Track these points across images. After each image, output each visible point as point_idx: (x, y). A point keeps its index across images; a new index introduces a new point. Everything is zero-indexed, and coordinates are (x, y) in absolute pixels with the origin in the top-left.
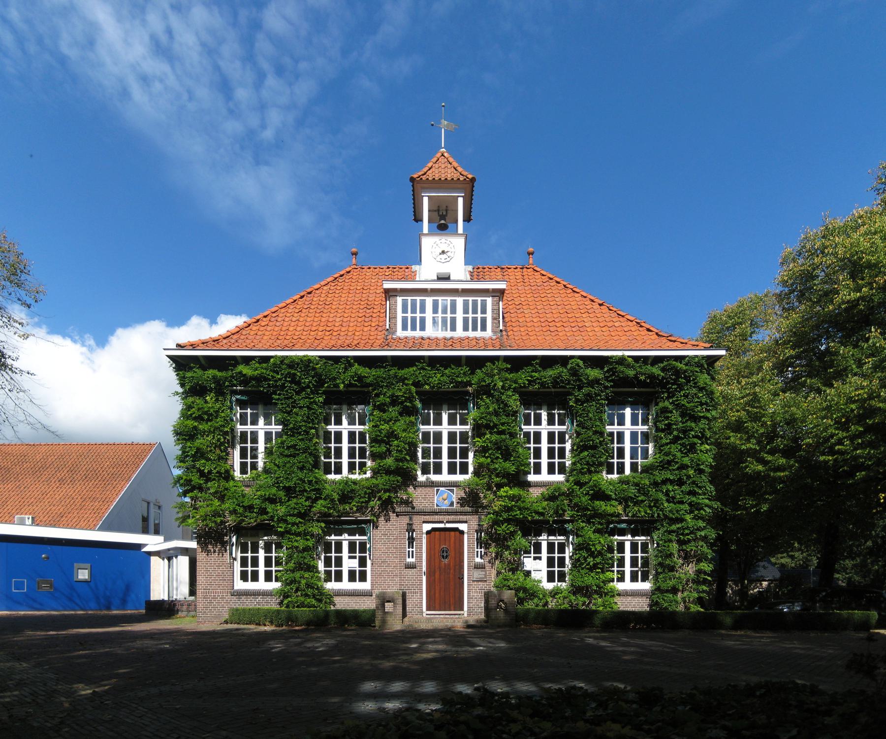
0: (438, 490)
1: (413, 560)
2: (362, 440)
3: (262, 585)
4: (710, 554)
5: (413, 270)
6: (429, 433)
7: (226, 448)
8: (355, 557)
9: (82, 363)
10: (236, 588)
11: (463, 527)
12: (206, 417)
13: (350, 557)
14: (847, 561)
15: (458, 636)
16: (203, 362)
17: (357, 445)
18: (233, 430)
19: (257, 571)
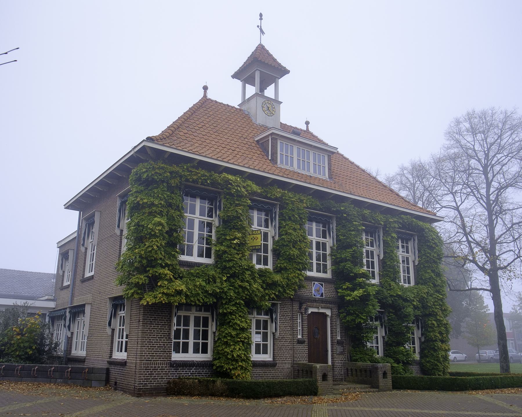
0: (314, 283)
1: (267, 358)
2: (177, 345)
3: (191, 356)
4: (481, 169)
5: (124, 287)
6: (320, 242)
7: (441, 324)
8: (259, 333)
9: (262, 69)
10: (114, 357)
11: (328, 312)
12: (148, 236)
13: (257, 333)
14: (246, 254)
15: (371, 176)
16: (149, 152)
17: (181, 341)
18: (249, 338)
19: (188, 343)
